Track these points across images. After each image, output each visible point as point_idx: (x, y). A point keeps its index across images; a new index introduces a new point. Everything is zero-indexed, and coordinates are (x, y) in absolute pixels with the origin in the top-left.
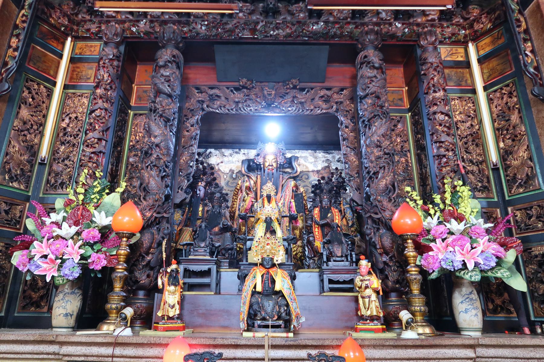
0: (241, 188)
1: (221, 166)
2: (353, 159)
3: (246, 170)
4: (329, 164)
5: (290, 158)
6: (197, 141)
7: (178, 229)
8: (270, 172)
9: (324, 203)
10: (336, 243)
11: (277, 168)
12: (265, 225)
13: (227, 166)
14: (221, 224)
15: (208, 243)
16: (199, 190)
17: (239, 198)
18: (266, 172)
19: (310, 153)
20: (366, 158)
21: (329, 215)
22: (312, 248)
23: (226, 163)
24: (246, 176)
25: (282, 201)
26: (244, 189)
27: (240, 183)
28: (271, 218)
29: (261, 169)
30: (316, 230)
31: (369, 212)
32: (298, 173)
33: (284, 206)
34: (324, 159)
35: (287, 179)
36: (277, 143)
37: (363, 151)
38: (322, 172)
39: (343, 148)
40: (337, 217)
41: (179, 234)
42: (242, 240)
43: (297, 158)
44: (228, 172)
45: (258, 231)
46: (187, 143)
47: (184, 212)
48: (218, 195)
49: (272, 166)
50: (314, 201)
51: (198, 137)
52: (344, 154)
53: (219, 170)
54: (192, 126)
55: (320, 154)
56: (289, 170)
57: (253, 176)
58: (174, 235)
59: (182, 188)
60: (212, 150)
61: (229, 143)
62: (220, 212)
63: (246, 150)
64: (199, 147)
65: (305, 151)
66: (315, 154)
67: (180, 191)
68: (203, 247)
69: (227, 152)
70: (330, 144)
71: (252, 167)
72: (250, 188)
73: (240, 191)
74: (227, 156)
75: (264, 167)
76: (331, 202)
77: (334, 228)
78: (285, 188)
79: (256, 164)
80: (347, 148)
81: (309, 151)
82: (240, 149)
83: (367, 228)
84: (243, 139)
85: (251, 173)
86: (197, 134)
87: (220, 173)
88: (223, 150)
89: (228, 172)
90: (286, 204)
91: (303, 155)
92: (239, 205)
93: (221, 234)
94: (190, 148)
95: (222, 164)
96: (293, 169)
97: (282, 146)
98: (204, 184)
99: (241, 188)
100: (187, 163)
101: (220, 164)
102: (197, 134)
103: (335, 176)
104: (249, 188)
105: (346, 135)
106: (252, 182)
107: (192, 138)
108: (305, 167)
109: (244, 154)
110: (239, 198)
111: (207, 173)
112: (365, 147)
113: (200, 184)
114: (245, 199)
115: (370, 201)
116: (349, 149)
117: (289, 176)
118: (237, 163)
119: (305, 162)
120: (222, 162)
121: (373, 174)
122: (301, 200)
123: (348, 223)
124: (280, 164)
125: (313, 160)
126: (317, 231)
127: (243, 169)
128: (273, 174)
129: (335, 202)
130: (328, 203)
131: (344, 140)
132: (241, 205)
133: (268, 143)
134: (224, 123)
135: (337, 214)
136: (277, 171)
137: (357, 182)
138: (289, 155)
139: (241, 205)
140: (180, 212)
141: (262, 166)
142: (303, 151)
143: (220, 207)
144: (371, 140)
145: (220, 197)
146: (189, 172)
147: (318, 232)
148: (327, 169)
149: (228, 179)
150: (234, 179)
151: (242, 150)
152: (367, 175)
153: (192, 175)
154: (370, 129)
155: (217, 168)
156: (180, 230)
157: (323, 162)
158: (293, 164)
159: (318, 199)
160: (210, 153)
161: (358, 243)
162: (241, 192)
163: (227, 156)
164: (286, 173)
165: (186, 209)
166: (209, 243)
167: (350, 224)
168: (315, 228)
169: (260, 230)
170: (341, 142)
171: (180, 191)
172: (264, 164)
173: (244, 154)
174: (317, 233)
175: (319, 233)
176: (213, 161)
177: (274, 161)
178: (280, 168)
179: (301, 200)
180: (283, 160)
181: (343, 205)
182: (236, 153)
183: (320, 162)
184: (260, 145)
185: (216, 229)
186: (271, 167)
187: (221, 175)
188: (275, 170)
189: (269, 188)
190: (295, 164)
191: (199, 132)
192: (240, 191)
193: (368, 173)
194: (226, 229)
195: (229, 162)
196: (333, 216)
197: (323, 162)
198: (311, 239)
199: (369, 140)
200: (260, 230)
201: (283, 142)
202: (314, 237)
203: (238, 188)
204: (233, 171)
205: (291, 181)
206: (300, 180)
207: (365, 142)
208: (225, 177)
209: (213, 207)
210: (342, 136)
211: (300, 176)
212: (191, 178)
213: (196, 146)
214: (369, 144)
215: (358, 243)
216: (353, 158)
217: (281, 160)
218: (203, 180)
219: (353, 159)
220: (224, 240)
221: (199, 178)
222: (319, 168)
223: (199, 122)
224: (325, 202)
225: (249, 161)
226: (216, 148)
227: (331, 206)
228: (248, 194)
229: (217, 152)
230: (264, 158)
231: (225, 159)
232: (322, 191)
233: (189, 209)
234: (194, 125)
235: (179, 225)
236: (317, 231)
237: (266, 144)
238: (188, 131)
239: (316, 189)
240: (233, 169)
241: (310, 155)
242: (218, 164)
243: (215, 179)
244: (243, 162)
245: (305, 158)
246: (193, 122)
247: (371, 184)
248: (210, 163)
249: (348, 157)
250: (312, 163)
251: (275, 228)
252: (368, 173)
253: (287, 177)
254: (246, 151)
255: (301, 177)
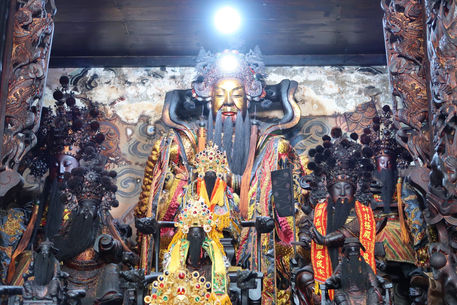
0: (159, 157)
1: (120, 107)
2: (413, 86)
3: (174, 116)
4: (374, 97)
5: (278, 87)
6: (48, 51)
7: (15, 256)
8: (228, 119)
9: (337, 192)
10: (355, 288)
11: (244, 110)
12: (187, 245)
13: (134, 106)
14: (97, 243)
15: (54, 288)
16: (66, 165)
17: (155, 181)
18: (218, 119)
19: (327, 73)
20: (437, 83)
21: (349, 220)
22: (308, 298)
23: (131, 98)
24: (172, 131)
25: (254, 188)
26: (166, 160)
27: (158, 147)
28: (201, 229)
29: (206, 113)
30: (319, 255)
31: (439, 211)
32: (296, 121)
33: (258, 198)
34: (361, 86)
35: (270, 135)
36: (245, 49)
37: (432, 65)
38: (358, 116)
39: (391, 59)
40: (368, 226)
41: (17, 266)
42: (131, 281)
43: (293, 86)
44: (136, 121)
45: (169, 260)
46: (23, 55)
47: (30, 216)
48: (90, 176)
49: (233, 104)
50: (313, 186)
51: (50, 40)
52: (395, 74)
53: (115, 116)
54: (36, 14)
55: (353, 75)
56: (277, 114)
57: (188, 128)
58: (5, 269)
59: (12, 161)
60: (100, 71)
61: (139, 53)
62: (96, 216)
63: (177, 69)
64: (53, 64)
65: (316, 68)
66: (341, 75)
67: (7, 168)
68: (44, 299)
69: (134, 74)
70: (365, 53)
71: (188, 108)
72: (180, 158)
73: (157, 165)
74: (135, 84)
75: (213, 108)
76: (354, 189)
77: (350, 250)
78: (261, 157)
79: (197, 102)
80: (398, 60)
81: (327, 68)
82: (163, 68)
83: (434, 250)
84: (170, 41)
85: (185, 124)
86: (47, 34)
87: (117, 123)
88: (125, 70)
89: (136, 121)
90: (263, 195)
91: (313, 77)
92: (155, 199)
93: (99, 266)
94: (32, 66)
95: (122, 103)
96: (285, 110)
97: (255, 57)
98: (75, 149)
99: (159, 157)
100: (24, 101)
101: (118, 103)
102: (47, 34)
103: (382, 127)
104: (177, 159)
105: (397, 29)
106: (187, 145)
107: (34, 43)
108: (316, 106)
109: (173, 77)
110: (155, 181)
111: (90, 125)
112: (435, 56)
113: (67, 149)
114: (169, 183)
115: (442, 186)
116: (404, 61)
117: (273, 129)
118: (156, 99)
119: (317, 93)
120: (122, 99)
121: (452, 120)
122: (288, 186)
123: (411, 239)
124: (252, 101)
125: (335, 89)
126: (320, 258)
127: (167, 113)
128: (234, 125)
129: (365, 189)
130: (348, 192)
131: (393, 39)
132: (160, 198)
133: (222, 50)
134: (119, 6)
135: (367, 217)
136: (244, 117)
137: (423, 139)
138: (274, 78)
139: (160, 198)
140: (21, 216)
141: (210, 106)
142: (312, 68)
143: (98, 203)
144: (448, 38)
145: (97, 181)
146: (28, 122)
147: (324, 260)
148: (369, 109)
149: (135, 137)
150: (150, 137)
151: (168, 69)
152: (438, 124)
153: (35, 129)
154: (446, 10)
155: (110, 112)
156: (19, 257)
157: (360, 92)
158: (285, 99)
159: (323, 183)
160: (95, 76)
161: (434, 286)
162: (161, 168)
163: (135, 84)
164: (268, 120)
165: (33, 209)
166: (58, 289)
167: (417, 239)
168: (316, 251)
169: (175, 257)
170: (387, 46)
171: (7, 168)
172: (213, 102)
173: (173, 77)
174: (319, 264)
175: (324, 264)
176: (101, 95)
177: (236, 93)
178: (251, 110)
179: (288, 186)
180: (259, 91)
181: (402, 195)
182: (156, 75)
183: (353, 93)
184: (204, 56)
185: (87, 256)
186: (229, 109)
187: (121, 128)
188: (240, 114)
189: (211, 159)
190: (288, 100)
191: (51, 29)
192: (157, 165)
193: (442, 117)
194: (107, 255)
195: (138, 96)
196: (357, 223)
197: (360, 92)
198: (306, 276)
199: (444, 38)
200: (175, 257)
201: (257, 48)
202: (313, 274)
203: (154, 158)
204: (149, 117)
205: (276, 141)
206: (305, 137)
207: (435, 43)
208: (129, 132)
209: (81, 203)
210: (388, 30)
211: (305, 128)
212: (34, 136)
213: (45, 63)
214: (445, 48)
215: (434, 286)
216: (413, 82)
217: (254, 92)
218: (73, 141)
219: (413, 86)
220: (103, 282)
221: (66, 136)
222: (351, 107)
223: (53, 6)
224: (341, 189)
225: (182, 94)
226: (108, 66)
227: (354, 199)
228: (175, 172)
229: (111, 75)
230: (214, 87)
231: (130, 91)
232: (332, 163)
233: (42, 209)
234: (39, 12)
235: (15, 247)
236: (320, 258)
237: (219, 54)
238: (25, 27)
239: (318, 160)
240: (147, 113)
241: (329, 78)
242: (113, 103)
243: (100, 139)
244: (169, 95)
245: (318, 84)
246: (37, 6)
247: (447, 145)
248: (94, 100)
249: (402, 80)
250: (330, 96)
251: (210, 251)
252: (442, 117)
253: (269, 131)
254: (178, 71)
255: (308, 130)
